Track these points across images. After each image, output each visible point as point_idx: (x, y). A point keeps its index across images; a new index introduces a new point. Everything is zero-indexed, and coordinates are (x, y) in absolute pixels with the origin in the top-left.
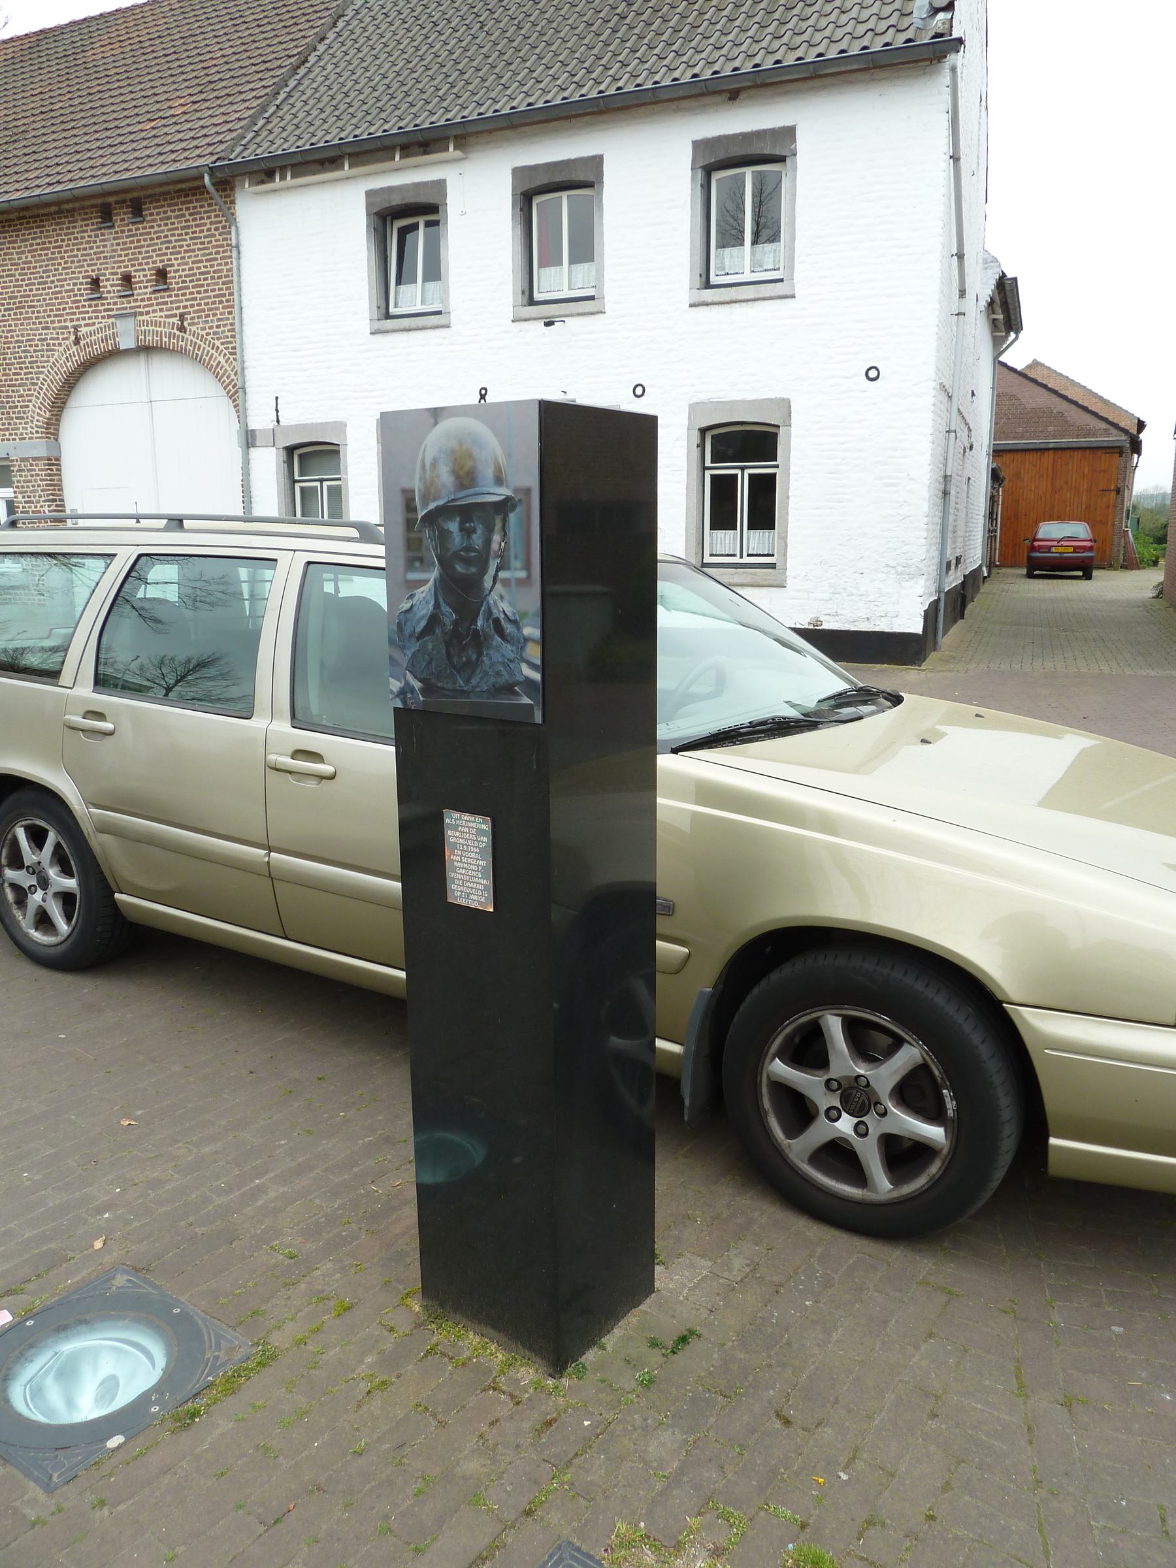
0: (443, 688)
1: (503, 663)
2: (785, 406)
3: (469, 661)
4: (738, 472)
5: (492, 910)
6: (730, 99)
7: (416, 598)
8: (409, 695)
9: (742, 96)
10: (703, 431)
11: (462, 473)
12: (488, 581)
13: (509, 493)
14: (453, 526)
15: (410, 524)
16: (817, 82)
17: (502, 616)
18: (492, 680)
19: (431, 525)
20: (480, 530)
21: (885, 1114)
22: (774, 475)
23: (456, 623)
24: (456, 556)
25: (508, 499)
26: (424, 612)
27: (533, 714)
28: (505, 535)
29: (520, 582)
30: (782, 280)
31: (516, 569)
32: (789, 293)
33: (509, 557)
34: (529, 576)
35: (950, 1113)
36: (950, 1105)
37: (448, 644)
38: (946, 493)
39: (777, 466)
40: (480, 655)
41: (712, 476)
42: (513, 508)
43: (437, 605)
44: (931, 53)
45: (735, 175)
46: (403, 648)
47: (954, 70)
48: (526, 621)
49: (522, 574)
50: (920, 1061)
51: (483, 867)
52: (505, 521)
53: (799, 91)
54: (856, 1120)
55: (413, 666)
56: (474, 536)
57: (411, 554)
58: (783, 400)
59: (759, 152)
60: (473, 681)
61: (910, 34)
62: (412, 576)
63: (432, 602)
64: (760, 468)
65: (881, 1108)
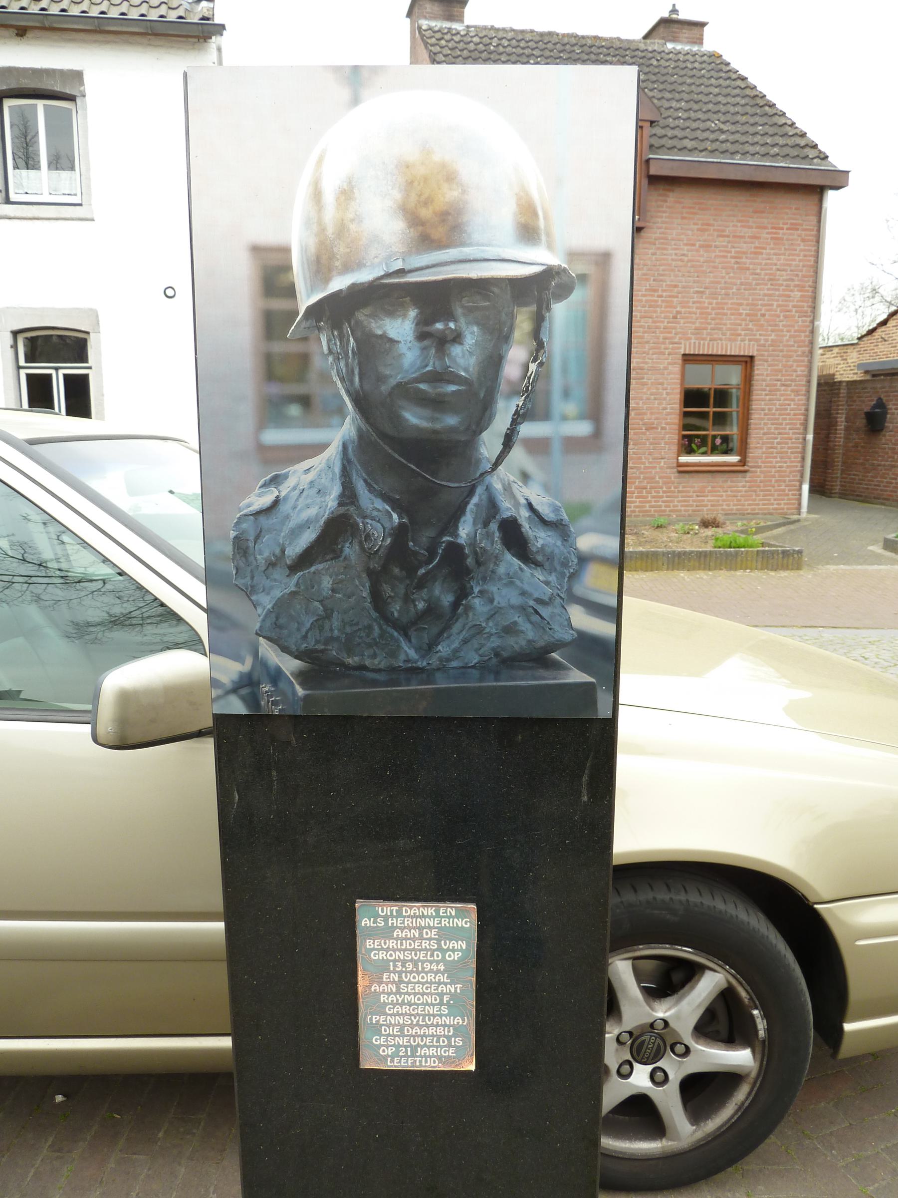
0: (363, 668)
1: (522, 609)
2: (94, 315)
3: (432, 611)
4: (53, 372)
5: (472, 1067)
6: (17, 35)
7: (291, 482)
8: (266, 688)
9: (29, 34)
10: (15, 334)
11: (425, 213)
12: (490, 443)
13: (554, 260)
14: (400, 328)
15: (273, 324)
16: (99, 37)
17: (524, 514)
18: (495, 642)
19: (336, 325)
20: (472, 336)
21: (688, 1051)
22: (86, 377)
23: (400, 534)
24: (406, 391)
25: (550, 273)
26: (312, 512)
27: (594, 703)
28: (539, 346)
29: (572, 444)
30: (80, 205)
31: (564, 418)
32: (89, 216)
33: (548, 394)
34: (598, 433)
35: (762, 1033)
36: (761, 1025)
37: (376, 578)
38: (871, 332)
39: (90, 368)
40: (463, 594)
41: (28, 375)
42: (564, 291)
43: (348, 496)
44: (200, 33)
45: (19, 106)
46: (249, 592)
47: (219, 49)
48: (585, 522)
49: (583, 429)
50: (724, 985)
51: (453, 996)
52: (539, 320)
53: (84, 41)
54: (650, 1068)
55: (277, 626)
56: (456, 350)
57: (275, 389)
58: (91, 310)
59: (50, 88)
60: (444, 649)
61: (181, 12)
62: (274, 436)
63: (336, 490)
64: (75, 369)
65: (680, 1049)
